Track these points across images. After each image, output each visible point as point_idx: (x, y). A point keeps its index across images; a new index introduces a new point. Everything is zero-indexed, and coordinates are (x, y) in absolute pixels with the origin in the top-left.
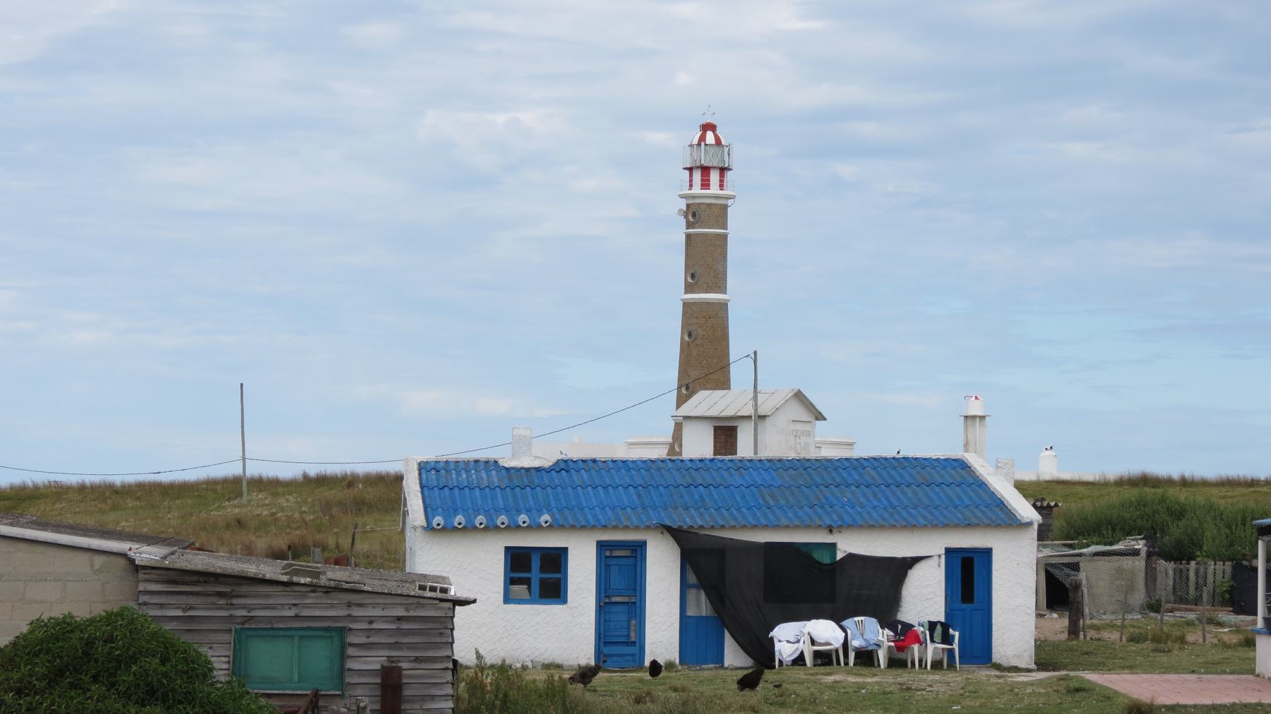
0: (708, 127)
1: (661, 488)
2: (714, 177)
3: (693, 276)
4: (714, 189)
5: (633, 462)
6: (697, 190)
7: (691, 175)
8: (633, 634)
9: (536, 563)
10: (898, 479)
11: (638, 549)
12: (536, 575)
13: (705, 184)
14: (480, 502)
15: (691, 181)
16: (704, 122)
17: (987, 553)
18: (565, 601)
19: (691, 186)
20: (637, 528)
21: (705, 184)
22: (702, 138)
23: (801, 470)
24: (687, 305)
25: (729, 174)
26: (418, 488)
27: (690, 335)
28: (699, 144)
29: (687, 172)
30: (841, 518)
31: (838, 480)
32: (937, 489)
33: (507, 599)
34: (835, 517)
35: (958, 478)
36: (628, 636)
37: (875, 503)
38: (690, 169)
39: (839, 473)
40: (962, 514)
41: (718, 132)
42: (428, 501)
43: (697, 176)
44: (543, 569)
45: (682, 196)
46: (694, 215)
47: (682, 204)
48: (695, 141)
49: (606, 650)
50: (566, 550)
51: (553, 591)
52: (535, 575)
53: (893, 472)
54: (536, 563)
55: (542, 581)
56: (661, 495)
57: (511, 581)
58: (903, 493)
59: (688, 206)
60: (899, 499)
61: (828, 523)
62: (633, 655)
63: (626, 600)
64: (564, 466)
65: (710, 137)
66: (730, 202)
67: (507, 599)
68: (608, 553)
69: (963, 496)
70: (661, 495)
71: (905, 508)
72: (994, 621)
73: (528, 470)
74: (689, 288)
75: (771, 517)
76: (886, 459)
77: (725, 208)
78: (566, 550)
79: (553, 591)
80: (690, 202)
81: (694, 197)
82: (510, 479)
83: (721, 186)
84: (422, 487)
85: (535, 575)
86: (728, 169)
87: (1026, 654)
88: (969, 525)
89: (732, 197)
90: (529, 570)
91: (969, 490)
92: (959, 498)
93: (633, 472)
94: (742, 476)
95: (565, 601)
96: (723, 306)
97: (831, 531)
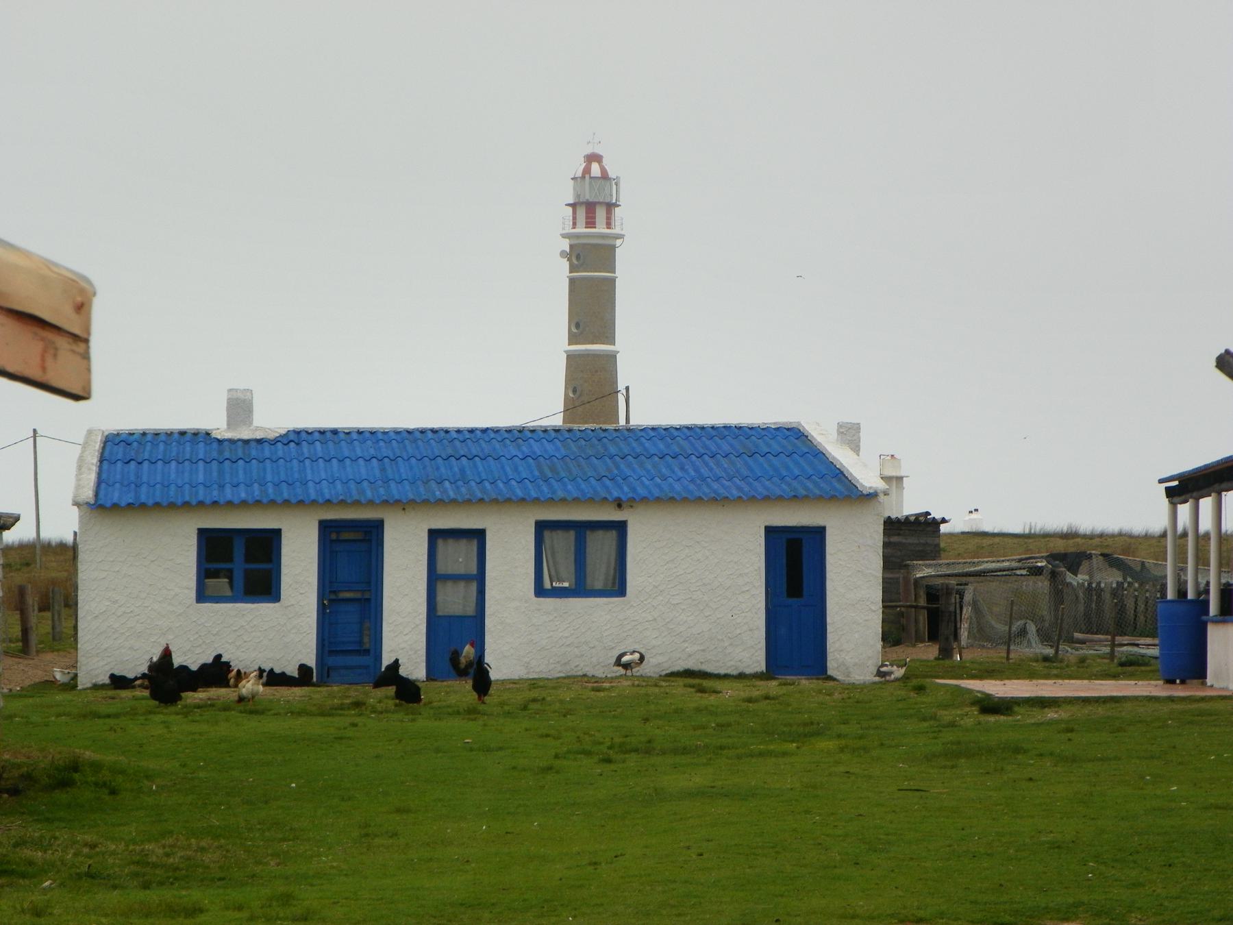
0: (593, 158)
1: (413, 460)
2: (601, 214)
3: (577, 325)
4: (601, 229)
5: (385, 433)
6: (581, 229)
7: (574, 213)
8: (366, 640)
9: (239, 551)
10: (714, 449)
11: (372, 533)
12: (238, 566)
13: (591, 223)
14: (173, 476)
15: (574, 218)
16: (589, 151)
17: (820, 532)
18: (277, 599)
19: (574, 225)
20: (371, 503)
21: (591, 223)
22: (587, 170)
23: (594, 441)
24: (571, 357)
25: (617, 211)
26: (95, 460)
27: (574, 391)
28: (583, 177)
29: (570, 209)
30: (634, 490)
31: (639, 450)
32: (761, 460)
33: (202, 597)
34: (626, 489)
35: (790, 448)
36: (361, 643)
37: (680, 474)
38: (574, 206)
39: (642, 444)
40: (789, 485)
41: (605, 162)
42: (104, 476)
43: (582, 213)
44: (249, 558)
45: (564, 236)
46: (578, 257)
47: (565, 245)
48: (579, 174)
49: (331, 661)
50: (278, 532)
51: (263, 586)
52: (239, 565)
53: (708, 442)
54: (239, 551)
55: (247, 573)
56: (411, 468)
57: (206, 572)
58: (718, 464)
59: (571, 246)
60: (711, 470)
61: (616, 494)
62: (367, 667)
63: (358, 595)
64: (296, 437)
65: (595, 169)
66: (618, 242)
67: (202, 597)
68: (334, 536)
69: (791, 465)
70: (411, 468)
71: (718, 479)
72: (829, 620)
73: (246, 442)
75: (545, 489)
76: (702, 428)
77: (613, 248)
78: (278, 532)
79: (263, 586)
80: (575, 242)
81: (578, 236)
82: (221, 452)
83: (609, 225)
84: (101, 461)
85: (239, 565)
86: (616, 205)
87: (870, 662)
88: (796, 498)
89: (621, 237)
90: (230, 560)
91: (801, 461)
92: (787, 468)
93: (382, 443)
94: (519, 446)
95: (277, 599)
96: (611, 358)
97: (620, 506)
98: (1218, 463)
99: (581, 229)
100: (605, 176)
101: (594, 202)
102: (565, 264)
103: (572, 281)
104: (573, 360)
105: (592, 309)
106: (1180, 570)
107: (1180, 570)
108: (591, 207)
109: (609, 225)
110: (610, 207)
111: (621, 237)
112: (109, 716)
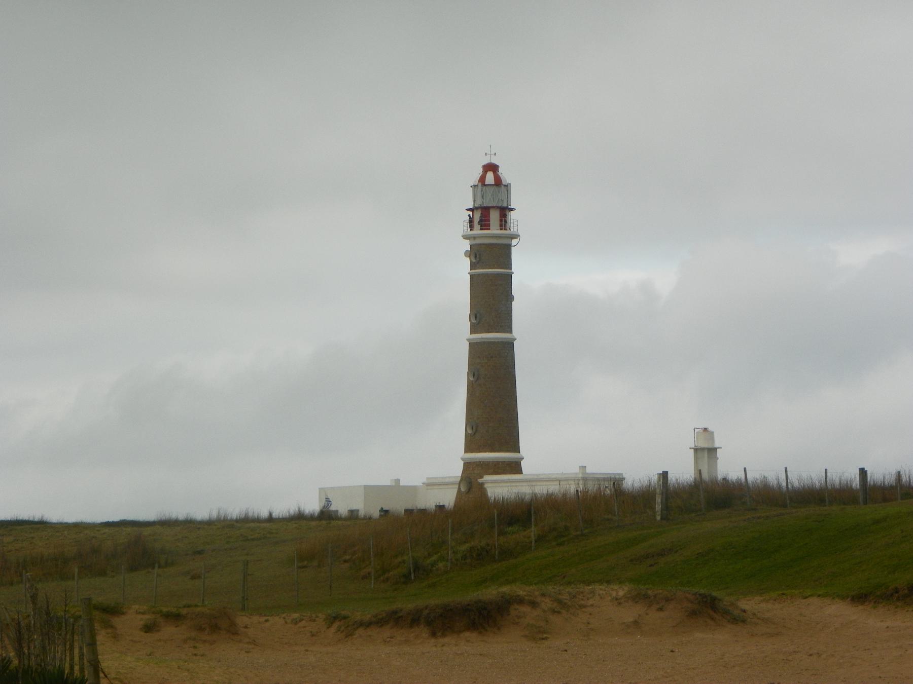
2: (494, 216)
4: (495, 230)
6: (477, 231)
16: (486, 161)
18: (320, 489)
22: (482, 179)
25: (512, 216)
45: (466, 237)
47: (466, 245)
66: (514, 242)
74: (474, 330)
77: (508, 248)
80: (478, 241)
81: (474, 237)
89: (515, 236)
98: (844, 470)
100: (498, 182)
102: (467, 262)
103: (472, 277)
104: (476, 349)
105: (492, 298)
106: (72, 668)
107: (72, 668)
108: (485, 211)
110: (505, 211)
111: (515, 236)
112: (253, 540)
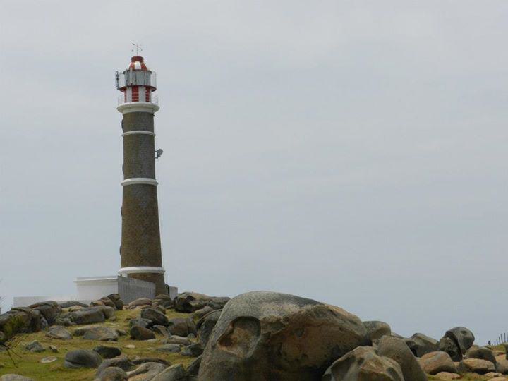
0: (140, 59)
2: (142, 93)
4: (142, 102)
6: (130, 103)
21: (135, 98)
22: (132, 67)
25: (153, 94)
43: (129, 92)
47: (120, 117)
77: (152, 115)
80: (125, 112)
99: (130, 103)
100: (144, 68)
101: (138, 84)
104: (128, 190)
108: (135, 88)
109: (148, 99)
110: (150, 89)
